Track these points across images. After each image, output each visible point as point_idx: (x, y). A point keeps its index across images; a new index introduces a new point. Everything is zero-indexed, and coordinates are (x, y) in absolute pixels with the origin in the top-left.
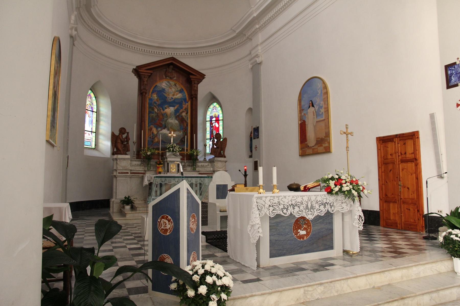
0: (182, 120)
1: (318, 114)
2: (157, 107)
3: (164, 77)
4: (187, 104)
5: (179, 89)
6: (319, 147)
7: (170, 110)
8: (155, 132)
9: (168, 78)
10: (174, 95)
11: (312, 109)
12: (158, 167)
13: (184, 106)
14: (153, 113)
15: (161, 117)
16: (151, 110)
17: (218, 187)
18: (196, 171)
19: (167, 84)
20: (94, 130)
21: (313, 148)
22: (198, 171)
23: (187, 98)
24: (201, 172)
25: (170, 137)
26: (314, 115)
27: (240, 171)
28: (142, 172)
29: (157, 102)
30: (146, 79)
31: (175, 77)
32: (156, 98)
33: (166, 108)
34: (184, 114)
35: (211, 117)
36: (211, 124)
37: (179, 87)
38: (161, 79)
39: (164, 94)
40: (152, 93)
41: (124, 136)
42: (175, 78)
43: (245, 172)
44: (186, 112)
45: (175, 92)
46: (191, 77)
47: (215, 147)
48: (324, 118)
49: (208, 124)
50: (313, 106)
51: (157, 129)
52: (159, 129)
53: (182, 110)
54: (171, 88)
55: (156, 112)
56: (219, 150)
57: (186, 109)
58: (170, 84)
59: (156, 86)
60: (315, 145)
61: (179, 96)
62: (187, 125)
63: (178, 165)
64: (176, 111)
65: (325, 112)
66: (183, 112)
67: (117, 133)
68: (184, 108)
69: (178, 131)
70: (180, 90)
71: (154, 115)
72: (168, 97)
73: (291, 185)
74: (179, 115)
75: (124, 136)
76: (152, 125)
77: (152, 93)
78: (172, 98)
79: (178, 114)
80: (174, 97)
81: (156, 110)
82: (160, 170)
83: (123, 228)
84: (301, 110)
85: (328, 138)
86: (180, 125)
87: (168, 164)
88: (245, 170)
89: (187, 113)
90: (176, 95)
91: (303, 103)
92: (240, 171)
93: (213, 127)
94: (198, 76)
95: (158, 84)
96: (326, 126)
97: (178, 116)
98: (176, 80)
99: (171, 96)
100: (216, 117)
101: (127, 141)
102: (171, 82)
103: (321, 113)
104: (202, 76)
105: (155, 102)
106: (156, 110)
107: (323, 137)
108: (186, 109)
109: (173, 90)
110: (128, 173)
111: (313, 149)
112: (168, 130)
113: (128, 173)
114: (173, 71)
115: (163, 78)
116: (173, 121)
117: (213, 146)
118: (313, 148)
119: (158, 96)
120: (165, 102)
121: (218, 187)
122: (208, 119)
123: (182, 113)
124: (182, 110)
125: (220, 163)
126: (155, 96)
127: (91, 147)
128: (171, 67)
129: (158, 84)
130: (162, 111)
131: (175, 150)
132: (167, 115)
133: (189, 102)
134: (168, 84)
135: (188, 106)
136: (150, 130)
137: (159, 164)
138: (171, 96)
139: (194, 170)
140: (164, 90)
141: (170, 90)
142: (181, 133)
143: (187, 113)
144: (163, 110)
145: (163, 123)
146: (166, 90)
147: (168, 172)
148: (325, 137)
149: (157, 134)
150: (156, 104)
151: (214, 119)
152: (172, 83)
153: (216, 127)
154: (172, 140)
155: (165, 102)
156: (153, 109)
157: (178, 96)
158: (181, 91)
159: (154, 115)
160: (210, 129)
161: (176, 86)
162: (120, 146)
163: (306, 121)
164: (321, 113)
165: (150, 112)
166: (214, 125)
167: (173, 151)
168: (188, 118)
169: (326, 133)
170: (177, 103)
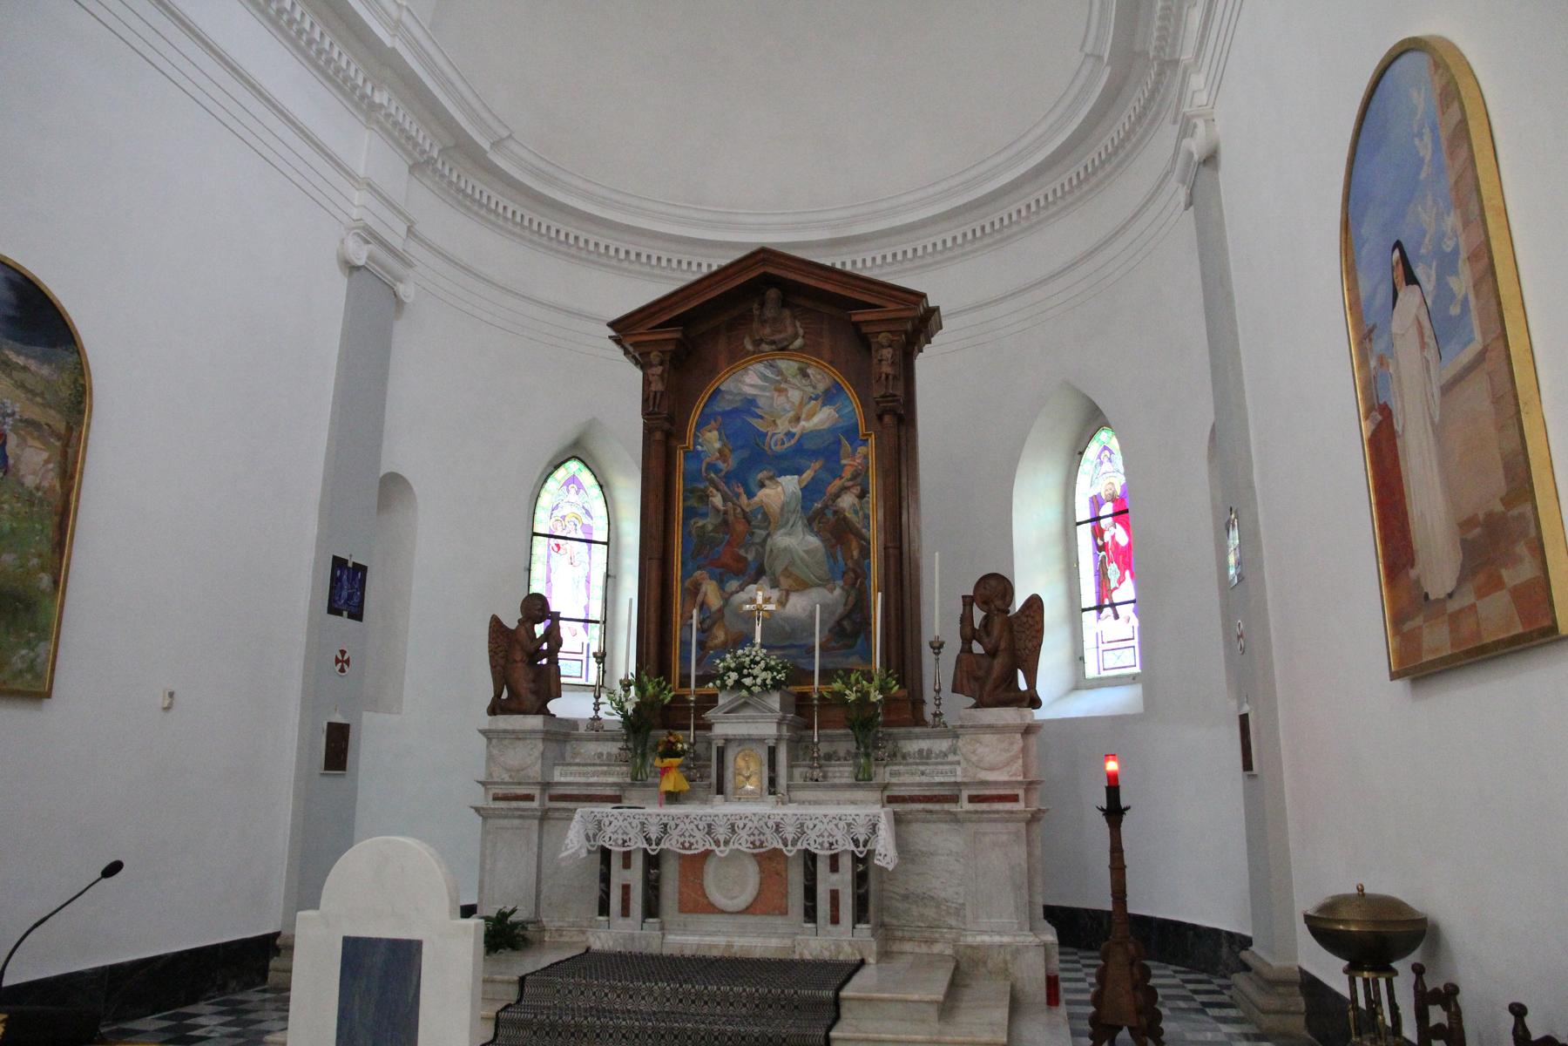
0: (838, 532)
1: (1440, 328)
2: (722, 486)
3: (750, 347)
4: (862, 450)
5: (821, 387)
6: (1481, 593)
7: (782, 491)
8: (715, 602)
9: (765, 347)
10: (797, 419)
11: (1409, 297)
12: (664, 771)
13: (849, 464)
14: (705, 515)
15: (740, 527)
16: (693, 502)
17: (356, 952)
18: (872, 788)
19: (764, 378)
20: (596, 614)
21: (1453, 606)
22: (885, 787)
23: (862, 428)
24: (896, 792)
25: (750, 618)
26: (1423, 345)
27: (113, 869)
28: (609, 792)
29: (721, 465)
30: (659, 370)
31: (796, 336)
32: (717, 445)
33: (762, 486)
34: (847, 501)
35: (1096, 502)
36: (1098, 533)
37: (821, 378)
38: (737, 357)
39: (755, 422)
40: (699, 426)
41: (539, 629)
42: (798, 342)
43: (1113, 790)
44: (857, 490)
45: (801, 405)
46: (859, 316)
47: (977, 648)
48: (1476, 346)
49: (1084, 534)
50: (1411, 279)
51: (721, 583)
52: (733, 585)
53: (837, 483)
54: (782, 392)
55: (718, 510)
56: (999, 664)
57: (860, 476)
58: (780, 373)
59: (717, 391)
60: (1461, 581)
61: (822, 418)
62: (865, 552)
63: (772, 752)
64: (810, 492)
65: (1477, 286)
66: (845, 489)
67: (511, 620)
68: (848, 474)
69: (824, 583)
70: (827, 392)
71: (709, 523)
72: (770, 430)
73: (1332, 907)
74: (826, 507)
75: (539, 629)
76: (699, 568)
77: (699, 426)
78: (790, 435)
79: (818, 505)
80: (796, 430)
81: (717, 500)
82: (668, 784)
83: (1094, 970)
84: (1366, 334)
85: (1526, 508)
86: (831, 555)
87: (721, 753)
88: (1113, 779)
89: (863, 495)
90: (810, 416)
91: (1364, 286)
92: (113, 869)
93: (1103, 548)
94: (892, 306)
95: (728, 385)
96: (1496, 400)
97: (821, 513)
98: (801, 349)
99: (783, 426)
100: (1114, 500)
101: (553, 653)
102: (782, 364)
103: (1455, 310)
104: (915, 321)
105: (712, 467)
106: (717, 500)
107: (1498, 507)
108: (860, 476)
109: (795, 395)
110: (529, 798)
111: (1455, 618)
112: (775, 584)
113: (529, 798)
114: (787, 313)
115: (748, 353)
116: (797, 542)
117: (966, 649)
118: (1453, 606)
119: (725, 436)
120: (757, 459)
121: (356, 952)
122: (1083, 512)
123: (838, 495)
124: (837, 483)
125: (988, 738)
126: (712, 441)
127: (582, 681)
128: (772, 294)
129: (728, 385)
130: (744, 497)
131: (748, 681)
132: (766, 516)
133: (872, 441)
134: (769, 373)
135: (866, 457)
136: (694, 591)
137: (664, 756)
138: (783, 426)
139: (863, 779)
140: (751, 402)
141: (780, 401)
142: (838, 591)
143: (863, 495)
144: (751, 495)
145: (750, 557)
146: (761, 402)
147: (720, 790)
148: (1508, 502)
149: (721, 610)
150: (717, 471)
151: (1108, 509)
152: (788, 366)
153: (1116, 545)
154: (758, 629)
155: (757, 459)
156: (704, 498)
157: (816, 420)
158: (828, 397)
159: (709, 523)
160: (1096, 556)
161: (805, 375)
162: (521, 675)
163: (1395, 406)
164: (1455, 310)
165: (690, 513)
166: (1107, 537)
167: (738, 685)
168: (867, 517)
169: (1508, 468)
170: (814, 454)
